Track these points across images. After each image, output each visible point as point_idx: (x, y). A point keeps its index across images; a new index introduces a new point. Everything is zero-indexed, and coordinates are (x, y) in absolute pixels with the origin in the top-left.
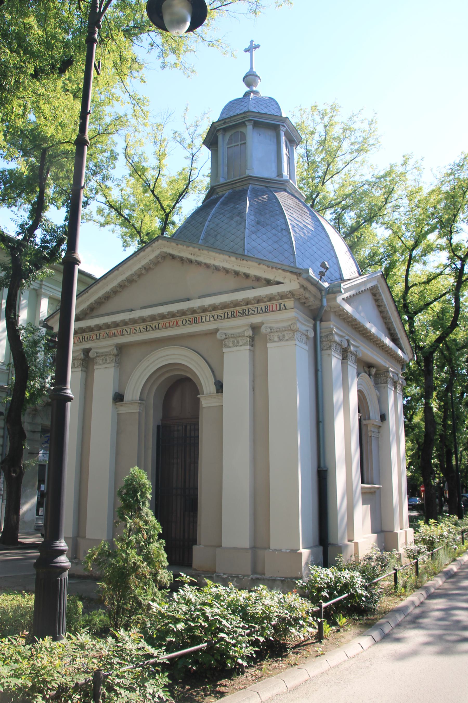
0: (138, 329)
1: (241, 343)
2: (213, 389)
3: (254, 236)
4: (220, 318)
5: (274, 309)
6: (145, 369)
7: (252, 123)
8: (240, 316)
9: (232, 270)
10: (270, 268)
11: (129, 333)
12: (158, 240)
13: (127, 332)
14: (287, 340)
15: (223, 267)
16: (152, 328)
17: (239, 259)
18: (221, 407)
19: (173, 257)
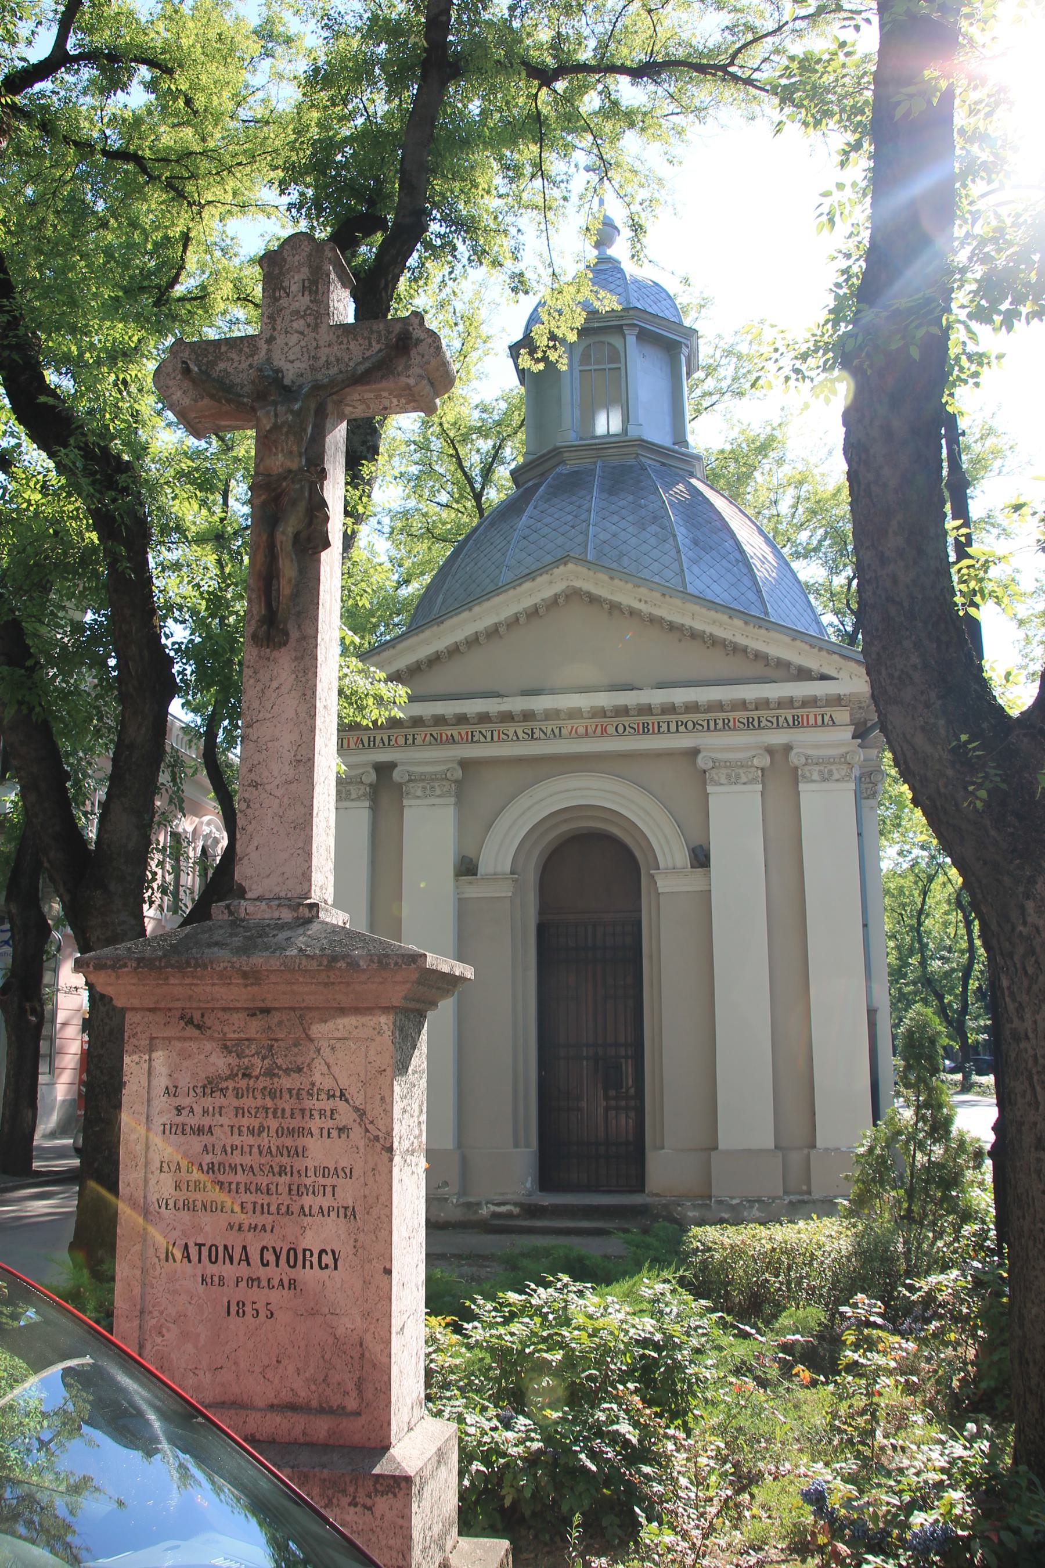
0: (511, 733)
1: (744, 779)
3: (695, 569)
5: (812, 721)
7: (636, 332)
10: (816, 650)
11: (489, 738)
12: (565, 564)
18: (706, 895)
19: (593, 599)
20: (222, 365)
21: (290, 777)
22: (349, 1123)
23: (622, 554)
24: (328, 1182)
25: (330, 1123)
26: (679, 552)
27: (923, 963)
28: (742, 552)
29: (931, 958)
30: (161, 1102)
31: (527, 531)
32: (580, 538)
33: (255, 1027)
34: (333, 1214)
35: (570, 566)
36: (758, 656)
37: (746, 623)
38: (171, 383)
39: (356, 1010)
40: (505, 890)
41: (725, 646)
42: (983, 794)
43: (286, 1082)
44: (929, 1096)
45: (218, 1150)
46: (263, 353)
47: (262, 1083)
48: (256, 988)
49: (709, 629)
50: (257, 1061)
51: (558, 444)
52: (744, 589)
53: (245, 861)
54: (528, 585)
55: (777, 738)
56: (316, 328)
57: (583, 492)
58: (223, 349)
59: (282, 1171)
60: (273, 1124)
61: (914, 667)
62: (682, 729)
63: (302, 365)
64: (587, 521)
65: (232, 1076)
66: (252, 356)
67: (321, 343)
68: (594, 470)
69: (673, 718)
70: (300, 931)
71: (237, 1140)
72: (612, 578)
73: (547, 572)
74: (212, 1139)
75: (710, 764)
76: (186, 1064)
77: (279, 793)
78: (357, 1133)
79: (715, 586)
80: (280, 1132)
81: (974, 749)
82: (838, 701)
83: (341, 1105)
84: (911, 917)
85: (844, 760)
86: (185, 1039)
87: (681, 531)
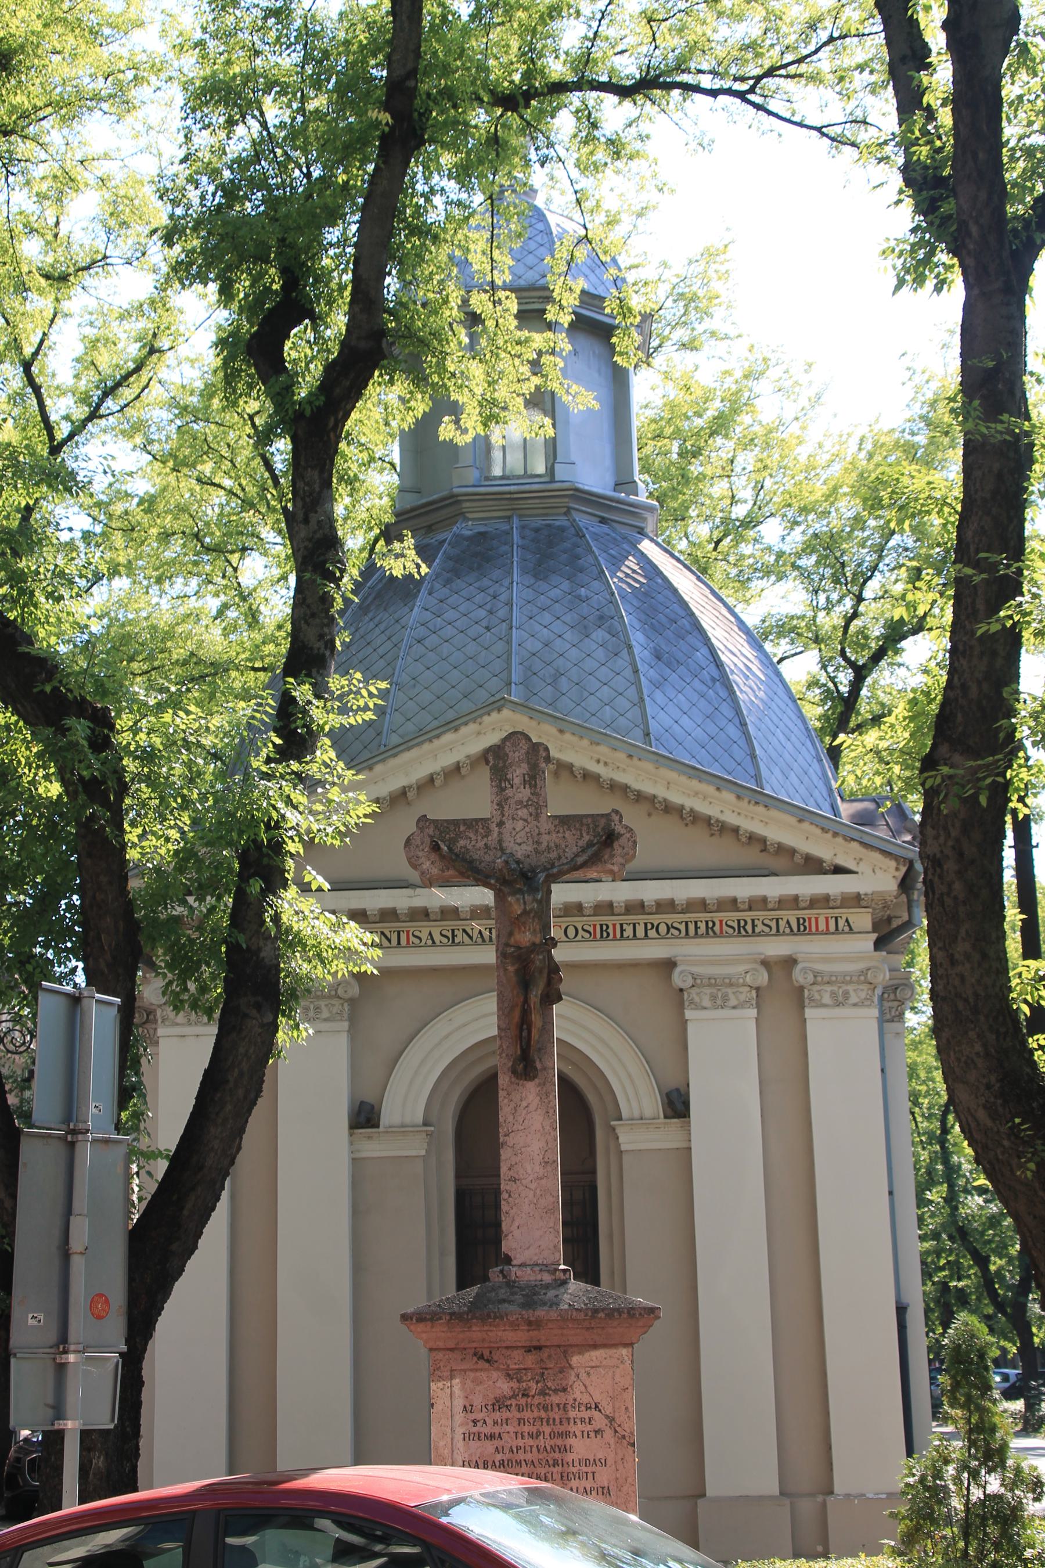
0: (424, 935)
1: (733, 1002)
2: (651, 1104)
3: (659, 696)
4: (676, 932)
5: (822, 926)
6: (439, 1043)
8: (731, 936)
9: (718, 821)
10: (829, 835)
11: (394, 942)
12: (499, 710)
13: (389, 941)
14: (855, 1005)
15: (692, 810)
16: (471, 938)
17: (746, 800)
20: (462, 843)
21: (541, 1175)
22: (603, 1427)
23: (559, 674)
24: (589, 1469)
25: (589, 1428)
26: (636, 671)
27: (951, 1199)
28: (719, 664)
29: (967, 1191)
30: (459, 1417)
31: (422, 631)
32: (500, 647)
33: (530, 1360)
34: (594, 1493)
35: (506, 712)
36: (753, 839)
37: (739, 797)
38: (420, 854)
39: (605, 1346)
40: (416, 1147)
41: (709, 824)
42: (1032, 1166)
43: (555, 1399)
44: (981, 1418)
45: (506, 1450)
46: (495, 835)
47: (537, 1400)
48: (536, 1332)
49: (689, 803)
50: (533, 1384)
51: (456, 491)
52: (723, 723)
53: (510, 1237)
54: (448, 737)
55: (776, 948)
56: (537, 817)
57: (496, 574)
58: (462, 828)
59: (555, 1463)
60: (547, 1430)
61: (978, 1054)
62: (652, 933)
63: (528, 848)
64: (508, 620)
65: (514, 1396)
66: (487, 836)
67: (542, 831)
68: (509, 533)
69: (641, 919)
70: (562, 1290)
71: (520, 1442)
72: (561, 731)
73: (474, 720)
74: (502, 1443)
75: (690, 981)
76: (478, 1388)
77: (533, 1186)
78: (608, 1434)
79: (685, 721)
80: (553, 1435)
81: (1025, 1130)
82: (856, 900)
83: (596, 1414)
84: (929, 1118)
85: (863, 977)
86: (476, 1370)
87: (637, 638)
